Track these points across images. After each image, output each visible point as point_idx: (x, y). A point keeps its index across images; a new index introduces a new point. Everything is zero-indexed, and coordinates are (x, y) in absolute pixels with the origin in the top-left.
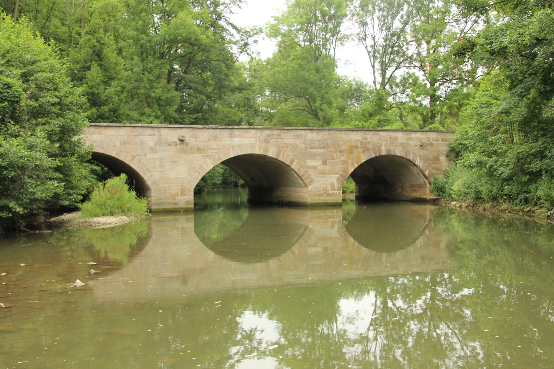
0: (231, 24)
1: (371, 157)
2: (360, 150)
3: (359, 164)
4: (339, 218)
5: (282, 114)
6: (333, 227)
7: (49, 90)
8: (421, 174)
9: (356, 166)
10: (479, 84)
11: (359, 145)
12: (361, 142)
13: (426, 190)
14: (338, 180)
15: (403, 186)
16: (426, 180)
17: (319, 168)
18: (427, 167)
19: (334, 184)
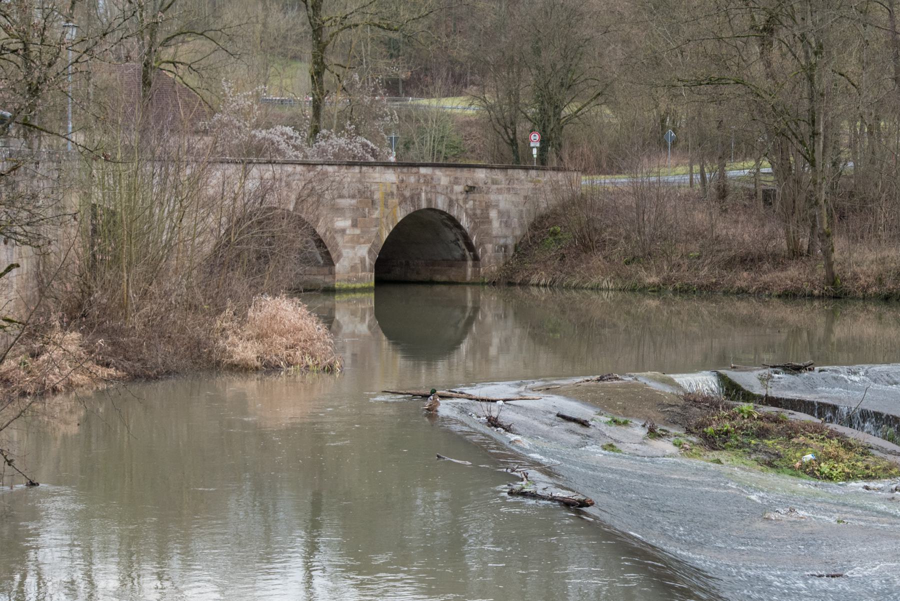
0: (865, 415)
1: (408, 213)
2: (396, 201)
3: (395, 225)
4: (371, 304)
5: (432, 179)
6: (363, 319)
7: (315, 165)
8: (461, 242)
9: (391, 228)
10: (737, 433)
11: (395, 192)
12: (398, 187)
13: (466, 271)
14: (370, 252)
15: (407, 264)
16: (467, 253)
17: (348, 232)
18: (474, 229)
19: (364, 258)
